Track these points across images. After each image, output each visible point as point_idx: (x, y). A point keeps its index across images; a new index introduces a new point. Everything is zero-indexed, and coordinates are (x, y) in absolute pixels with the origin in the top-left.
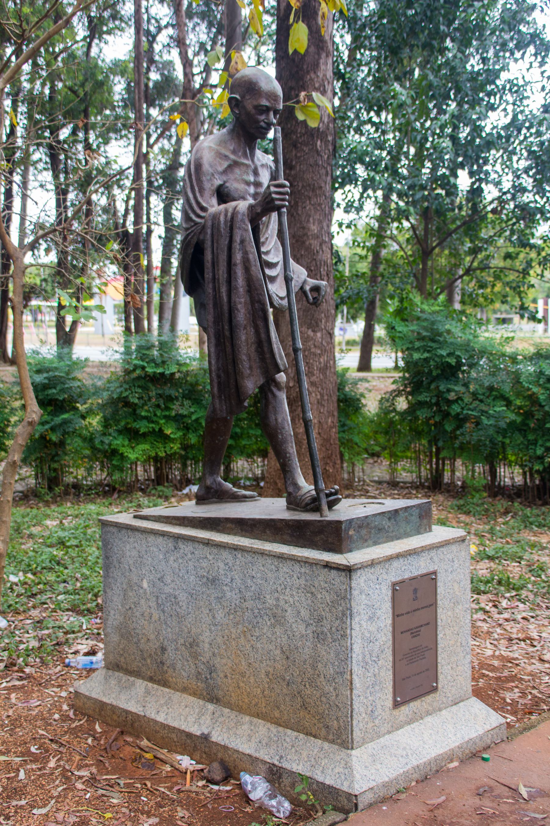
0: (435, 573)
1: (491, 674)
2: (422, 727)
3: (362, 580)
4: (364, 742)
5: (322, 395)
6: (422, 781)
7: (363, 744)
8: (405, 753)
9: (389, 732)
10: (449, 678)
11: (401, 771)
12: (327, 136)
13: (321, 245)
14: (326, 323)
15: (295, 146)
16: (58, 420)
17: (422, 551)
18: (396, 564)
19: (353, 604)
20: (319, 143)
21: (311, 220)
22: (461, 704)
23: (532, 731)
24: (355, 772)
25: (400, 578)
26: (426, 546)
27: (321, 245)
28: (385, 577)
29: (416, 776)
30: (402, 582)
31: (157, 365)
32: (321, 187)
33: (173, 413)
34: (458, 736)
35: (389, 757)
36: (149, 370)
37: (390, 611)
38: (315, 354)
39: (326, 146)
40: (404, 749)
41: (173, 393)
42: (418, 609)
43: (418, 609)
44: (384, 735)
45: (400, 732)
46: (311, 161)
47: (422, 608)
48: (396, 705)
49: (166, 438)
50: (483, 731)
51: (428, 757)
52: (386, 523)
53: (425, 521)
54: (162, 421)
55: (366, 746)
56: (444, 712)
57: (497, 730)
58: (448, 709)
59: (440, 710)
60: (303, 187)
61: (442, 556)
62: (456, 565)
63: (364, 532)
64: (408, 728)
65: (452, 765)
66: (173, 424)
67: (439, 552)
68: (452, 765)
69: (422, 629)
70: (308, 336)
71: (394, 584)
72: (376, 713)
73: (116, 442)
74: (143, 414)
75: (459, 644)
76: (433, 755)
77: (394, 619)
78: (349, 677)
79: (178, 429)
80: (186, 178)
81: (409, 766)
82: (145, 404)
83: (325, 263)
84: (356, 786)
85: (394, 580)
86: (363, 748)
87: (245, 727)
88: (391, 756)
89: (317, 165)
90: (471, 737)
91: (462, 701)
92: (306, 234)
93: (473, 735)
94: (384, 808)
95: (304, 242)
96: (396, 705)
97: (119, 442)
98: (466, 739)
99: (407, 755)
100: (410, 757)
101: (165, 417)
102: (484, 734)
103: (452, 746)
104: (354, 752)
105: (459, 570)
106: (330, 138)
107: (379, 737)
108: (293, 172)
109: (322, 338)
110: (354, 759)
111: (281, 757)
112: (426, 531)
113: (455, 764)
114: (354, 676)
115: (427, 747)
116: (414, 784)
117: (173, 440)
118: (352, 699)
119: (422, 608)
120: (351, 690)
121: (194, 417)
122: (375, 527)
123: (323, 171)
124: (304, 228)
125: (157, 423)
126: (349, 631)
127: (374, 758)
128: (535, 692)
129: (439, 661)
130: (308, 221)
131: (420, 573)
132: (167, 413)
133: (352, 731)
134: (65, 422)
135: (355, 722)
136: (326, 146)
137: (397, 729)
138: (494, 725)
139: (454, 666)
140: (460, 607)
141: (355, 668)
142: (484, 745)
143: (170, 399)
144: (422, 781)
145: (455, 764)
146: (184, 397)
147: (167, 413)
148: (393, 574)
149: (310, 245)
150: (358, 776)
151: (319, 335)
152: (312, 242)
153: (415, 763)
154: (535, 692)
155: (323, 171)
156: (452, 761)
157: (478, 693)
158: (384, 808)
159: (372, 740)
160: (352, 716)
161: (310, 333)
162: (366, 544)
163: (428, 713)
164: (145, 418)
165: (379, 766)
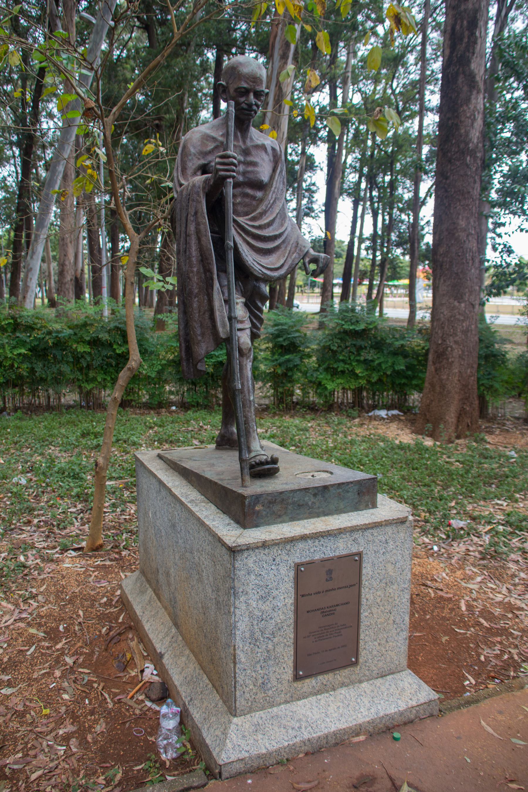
0: (360, 554)
1: (485, 624)
2: (332, 698)
3: (250, 562)
4: (251, 710)
5: (463, 351)
6: (313, 754)
7: (249, 712)
8: (298, 725)
9: (286, 702)
10: (375, 652)
11: (286, 744)
12: (476, 153)
13: (468, 236)
14: (469, 296)
15: (450, 161)
16: (283, 359)
17: (340, 533)
18: (301, 545)
19: (237, 584)
20: (468, 158)
21: (460, 217)
22: (389, 677)
23: (472, 707)
24: (228, 741)
25: (308, 559)
26: (345, 529)
27: (468, 236)
28: (286, 558)
29: (305, 748)
30: (311, 563)
31: (352, 324)
32: (469, 192)
33: (362, 358)
34: (372, 710)
35: (276, 728)
36: (346, 327)
37: (292, 591)
38: (459, 320)
39: (475, 161)
40: (299, 720)
41: (363, 343)
42: (333, 589)
43: (333, 589)
44: (280, 704)
45: (300, 703)
46: (462, 172)
47: (339, 588)
48: (297, 678)
49: (357, 377)
50: (405, 707)
51: (326, 731)
52: (309, 499)
53: (367, 498)
54: (354, 364)
55: (253, 714)
56: (364, 685)
57: (425, 706)
58: (371, 682)
59: (360, 682)
60: (455, 192)
61: (370, 538)
62: (391, 545)
63: (276, 508)
64: (313, 699)
65: (356, 739)
66: (363, 366)
67: (366, 533)
68: (356, 739)
69: (338, 608)
70: (454, 306)
71: (298, 566)
72: (269, 685)
73: (322, 376)
74: (341, 358)
75: (391, 622)
76: (332, 730)
77: (297, 599)
78: (232, 652)
79: (367, 370)
80: (337, 190)
81: (298, 740)
82: (343, 351)
83: (471, 250)
84: (224, 756)
85: (297, 561)
86: (248, 716)
87: (184, 659)
88: (280, 727)
89: (466, 175)
90: (388, 712)
91: (393, 673)
92: (456, 228)
93: (392, 710)
94: (250, 781)
95: (454, 234)
96: (297, 678)
97: (322, 376)
98: (381, 714)
99: (300, 728)
100: (303, 730)
101: (358, 361)
102: (405, 710)
103: (361, 720)
104: (235, 720)
105: (394, 551)
106: (479, 155)
107: (273, 706)
108: (448, 182)
109: (465, 308)
110: (233, 727)
111: (191, 699)
112: (367, 507)
113: (362, 738)
114: (238, 652)
115: (328, 720)
116: (301, 755)
117: (361, 378)
118: (235, 673)
119: (339, 588)
120: (235, 663)
121: (377, 362)
122: (294, 503)
123: (471, 180)
124: (454, 223)
125: (350, 364)
126: (232, 609)
127: (257, 728)
128: (514, 651)
129: (362, 636)
130: (458, 218)
131: (337, 554)
132: (358, 358)
133: (235, 701)
134: (289, 360)
135: (238, 693)
136: (475, 161)
137: (299, 699)
138: (422, 701)
139: (383, 642)
140: (395, 587)
141: (239, 643)
142: (404, 720)
143: (360, 349)
144: (313, 754)
145: (362, 738)
146: (372, 347)
147: (358, 358)
148: (298, 555)
149: (459, 236)
150: (229, 745)
151: (463, 305)
152: (460, 234)
153: (306, 736)
154: (514, 651)
155: (471, 180)
156: (358, 735)
157: (409, 666)
158: (250, 781)
159: (263, 708)
160: (235, 687)
161: (456, 303)
162: (280, 520)
163: (343, 685)
164: (343, 361)
165: (260, 736)
